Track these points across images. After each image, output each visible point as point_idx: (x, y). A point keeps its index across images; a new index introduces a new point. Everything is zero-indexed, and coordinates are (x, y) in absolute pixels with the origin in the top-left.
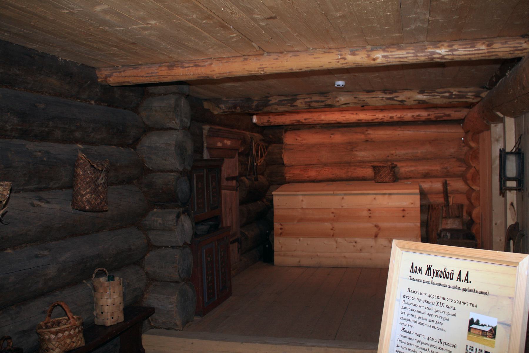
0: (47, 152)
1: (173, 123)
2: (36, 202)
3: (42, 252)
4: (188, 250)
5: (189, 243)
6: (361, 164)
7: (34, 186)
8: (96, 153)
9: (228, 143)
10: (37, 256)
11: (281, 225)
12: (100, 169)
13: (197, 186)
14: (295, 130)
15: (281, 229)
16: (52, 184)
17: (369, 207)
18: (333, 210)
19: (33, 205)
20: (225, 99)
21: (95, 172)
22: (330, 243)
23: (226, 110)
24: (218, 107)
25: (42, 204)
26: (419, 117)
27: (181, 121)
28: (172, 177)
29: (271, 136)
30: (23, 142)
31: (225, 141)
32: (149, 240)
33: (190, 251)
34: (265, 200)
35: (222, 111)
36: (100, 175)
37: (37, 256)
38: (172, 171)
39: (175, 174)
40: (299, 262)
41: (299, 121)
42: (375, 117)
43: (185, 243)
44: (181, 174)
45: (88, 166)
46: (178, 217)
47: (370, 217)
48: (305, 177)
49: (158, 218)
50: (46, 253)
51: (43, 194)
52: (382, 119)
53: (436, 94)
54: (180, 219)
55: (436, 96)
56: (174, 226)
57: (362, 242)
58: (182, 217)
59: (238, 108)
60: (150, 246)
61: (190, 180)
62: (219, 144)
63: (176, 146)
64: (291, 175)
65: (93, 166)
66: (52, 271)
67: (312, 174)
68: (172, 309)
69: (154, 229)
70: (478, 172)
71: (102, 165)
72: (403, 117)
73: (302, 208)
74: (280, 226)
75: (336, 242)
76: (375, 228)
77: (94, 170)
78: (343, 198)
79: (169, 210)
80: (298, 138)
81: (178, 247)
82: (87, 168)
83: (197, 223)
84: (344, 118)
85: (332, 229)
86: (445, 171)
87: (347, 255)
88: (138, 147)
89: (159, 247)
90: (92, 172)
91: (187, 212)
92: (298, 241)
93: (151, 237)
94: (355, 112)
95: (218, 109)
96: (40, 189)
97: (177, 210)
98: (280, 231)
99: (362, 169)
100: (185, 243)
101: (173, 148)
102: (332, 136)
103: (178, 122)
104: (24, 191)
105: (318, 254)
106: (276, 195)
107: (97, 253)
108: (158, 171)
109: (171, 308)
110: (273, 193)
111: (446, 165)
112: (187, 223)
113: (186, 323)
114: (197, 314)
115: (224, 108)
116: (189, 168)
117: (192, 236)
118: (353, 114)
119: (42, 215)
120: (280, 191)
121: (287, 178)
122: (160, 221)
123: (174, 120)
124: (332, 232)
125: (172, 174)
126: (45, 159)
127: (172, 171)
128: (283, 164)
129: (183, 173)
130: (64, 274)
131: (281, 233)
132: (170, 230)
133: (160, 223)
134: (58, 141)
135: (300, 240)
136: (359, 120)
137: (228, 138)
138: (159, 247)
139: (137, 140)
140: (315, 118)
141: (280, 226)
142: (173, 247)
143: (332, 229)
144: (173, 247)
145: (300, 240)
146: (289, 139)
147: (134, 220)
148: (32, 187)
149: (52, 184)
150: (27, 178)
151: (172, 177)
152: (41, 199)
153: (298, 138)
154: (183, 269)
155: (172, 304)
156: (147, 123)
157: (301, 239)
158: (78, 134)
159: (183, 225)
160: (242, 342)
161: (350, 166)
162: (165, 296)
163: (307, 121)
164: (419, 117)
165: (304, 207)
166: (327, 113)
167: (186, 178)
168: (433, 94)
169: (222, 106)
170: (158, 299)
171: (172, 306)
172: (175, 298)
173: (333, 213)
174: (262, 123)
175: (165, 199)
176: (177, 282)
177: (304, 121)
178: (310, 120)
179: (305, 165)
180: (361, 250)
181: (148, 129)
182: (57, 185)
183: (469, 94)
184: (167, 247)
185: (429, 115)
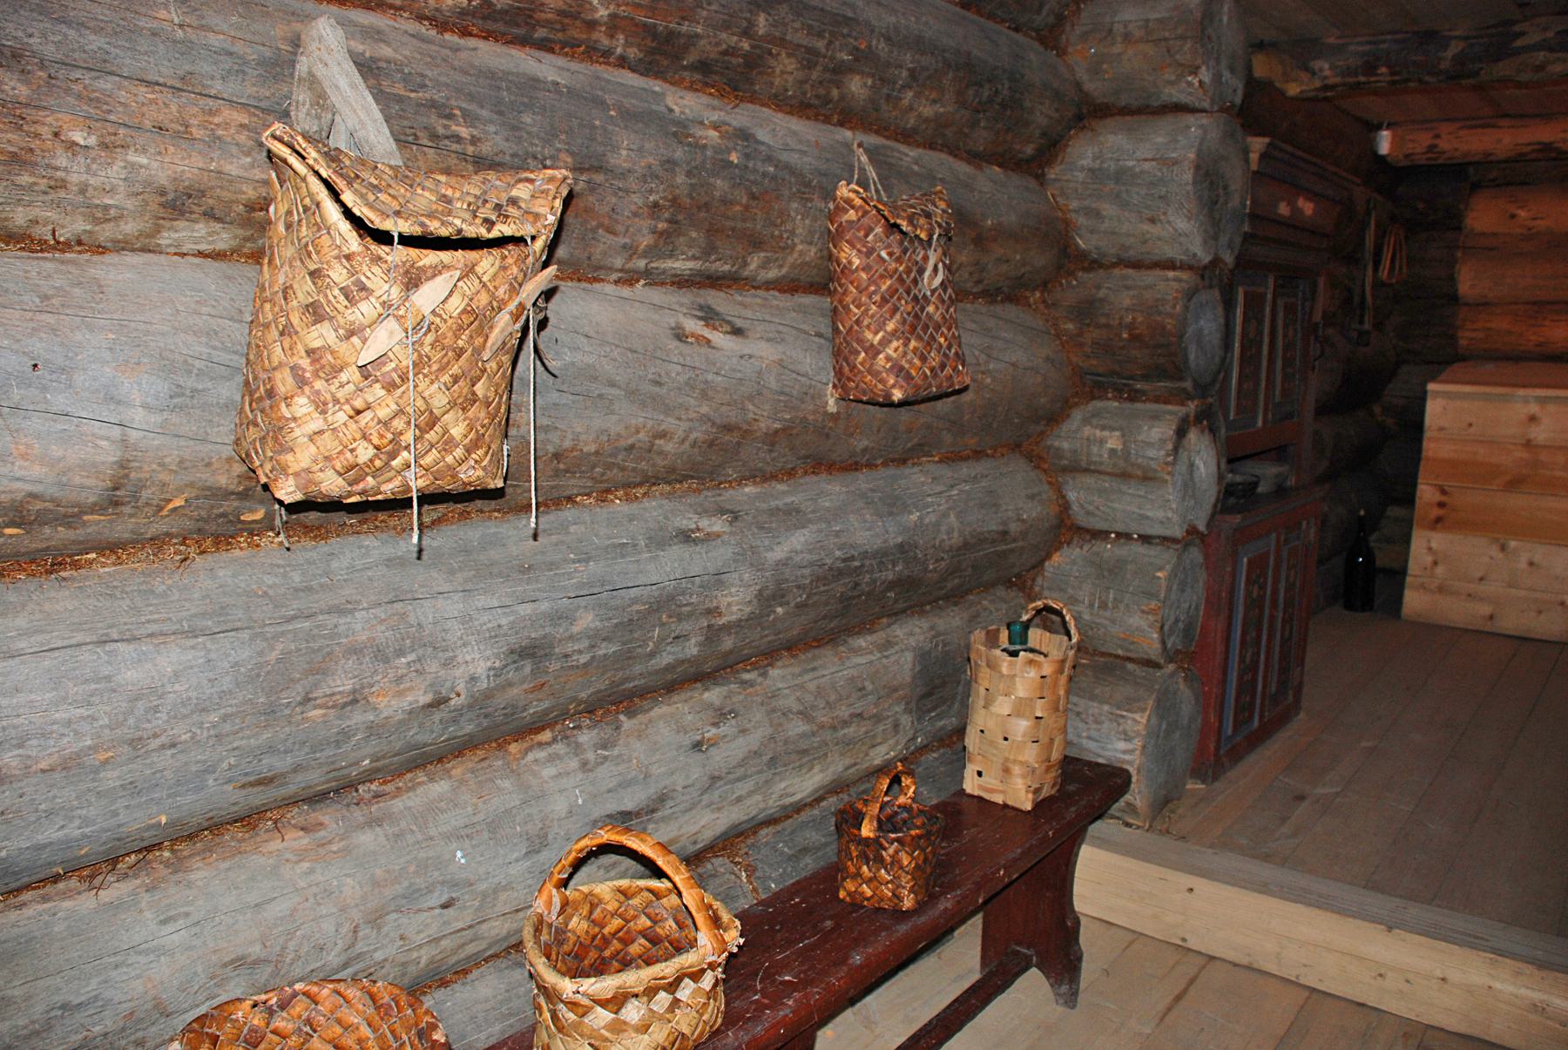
0: (744, 135)
1: (1190, 84)
2: (693, 325)
3: (704, 523)
4: (1195, 554)
5: (1202, 528)
7: (690, 265)
8: (916, 168)
9: (1307, 207)
10: (686, 537)
11: (1444, 492)
12: (923, 236)
13: (1244, 335)
15: (1441, 505)
16: (754, 262)
19: (680, 335)
20: (1331, 40)
21: (905, 251)
23: (1331, 81)
24: (1307, 69)
25: (717, 337)
27: (1217, 78)
28: (1169, 285)
29: (1421, 206)
30: (657, 86)
31: (1301, 203)
32: (1065, 507)
33: (1201, 560)
34: (1377, 409)
35: (1318, 84)
36: (926, 258)
37: (686, 537)
38: (1170, 265)
39: (1184, 275)
40: (1491, 617)
43: (1192, 531)
44: (1202, 277)
45: (878, 230)
46: (1181, 433)
49: (1096, 433)
50: (718, 525)
51: (717, 299)
54: (1185, 442)
56: (1167, 464)
58: (1193, 436)
59: (1384, 70)
60: (1065, 528)
61: (1229, 305)
62: (1283, 209)
63: (1197, 168)
65: (896, 226)
66: (735, 601)
68: (1127, 757)
69: (1086, 470)
71: (928, 216)
74: (1438, 497)
77: (901, 243)
79: (1149, 406)
81: (1166, 540)
82: (878, 239)
83: (1233, 457)
88: (1052, 173)
89: (1100, 535)
90: (897, 251)
91: (1205, 419)
93: (1072, 496)
95: (1304, 76)
96: (713, 281)
97: (1181, 410)
98: (1436, 512)
100: (1192, 531)
101: (1188, 176)
103: (1206, 80)
104: (653, 279)
106: (1437, 394)
107: (900, 540)
108: (1122, 262)
109: (1125, 752)
110: (1431, 387)
112: (1203, 459)
113: (1164, 803)
114: (1198, 772)
115: (1327, 73)
116: (1229, 258)
117: (1215, 506)
119: (710, 377)
120: (1447, 382)
121: (1463, 342)
122: (1113, 442)
123: (1195, 73)
125: (1171, 274)
126: (734, 158)
127: (1170, 265)
128: (1454, 298)
129: (1206, 272)
130: (779, 610)
131: (1439, 520)
132: (1148, 478)
133: (1113, 451)
134: (780, 102)
137: (1311, 195)
138: (1100, 535)
139: (1051, 148)
141: (1438, 497)
142: (1145, 539)
144: (1145, 539)
146: (1483, 216)
147: (1020, 432)
148: (682, 265)
149: (754, 262)
150: (661, 226)
151: (1169, 285)
152: (709, 316)
154: (1177, 620)
155: (1128, 739)
156: (1090, 86)
157: (1513, 544)
158: (857, 87)
159: (1191, 465)
160: (1390, 929)
162: (1106, 708)
167: (1216, 293)
169: (1323, 66)
170: (1078, 714)
171: (1129, 746)
172: (1142, 718)
174: (1407, 156)
175: (1127, 367)
176: (1149, 663)
179: (1534, 303)
181: (1089, 112)
182: (772, 274)
184: (1124, 536)
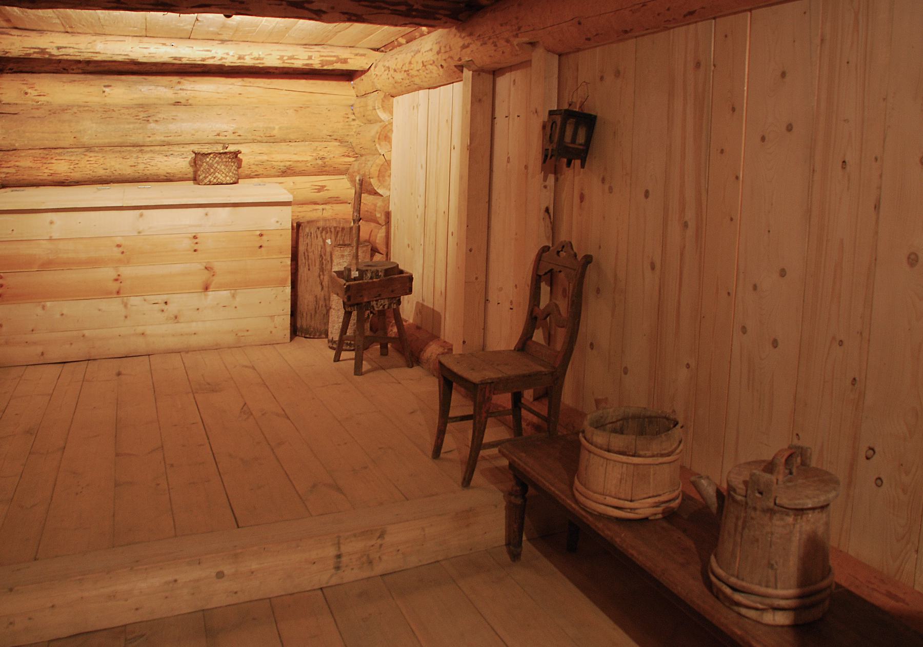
6: (165, 148)
14: (21, 72)
17: (194, 230)
18: (119, 240)
22: (113, 306)
26: (292, 61)
40: (42, 354)
41: (43, 51)
42: (209, 54)
47: (195, 251)
48: (44, 173)
52: (222, 59)
53: (384, 5)
55: (384, 8)
57: (178, 302)
64: (12, 170)
67: (61, 167)
70: (388, 163)
72: (263, 59)
73: (51, 239)
75: (126, 305)
76: (206, 271)
78: (141, 215)
80: (29, 91)
84: (146, 52)
85: (116, 280)
86: (320, 162)
87: (149, 330)
92: (39, 310)
94: (168, 42)
99: (165, 158)
102: (107, 90)
105: (87, 333)
111: (321, 153)
118: (164, 44)
124: (115, 286)
135: (44, 307)
136: (175, 58)
140: (82, 46)
143: (116, 280)
145: (44, 307)
153: (29, 91)
157: (48, 304)
161: (141, 151)
163: (63, 51)
164: (292, 61)
165: (55, 236)
166: (109, 38)
168: (378, 4)
173: (119, 246)
177: (55, 52)
178: (71, 51)
180: (176, 317)
183: (441, 12)
185: (310, 58)
